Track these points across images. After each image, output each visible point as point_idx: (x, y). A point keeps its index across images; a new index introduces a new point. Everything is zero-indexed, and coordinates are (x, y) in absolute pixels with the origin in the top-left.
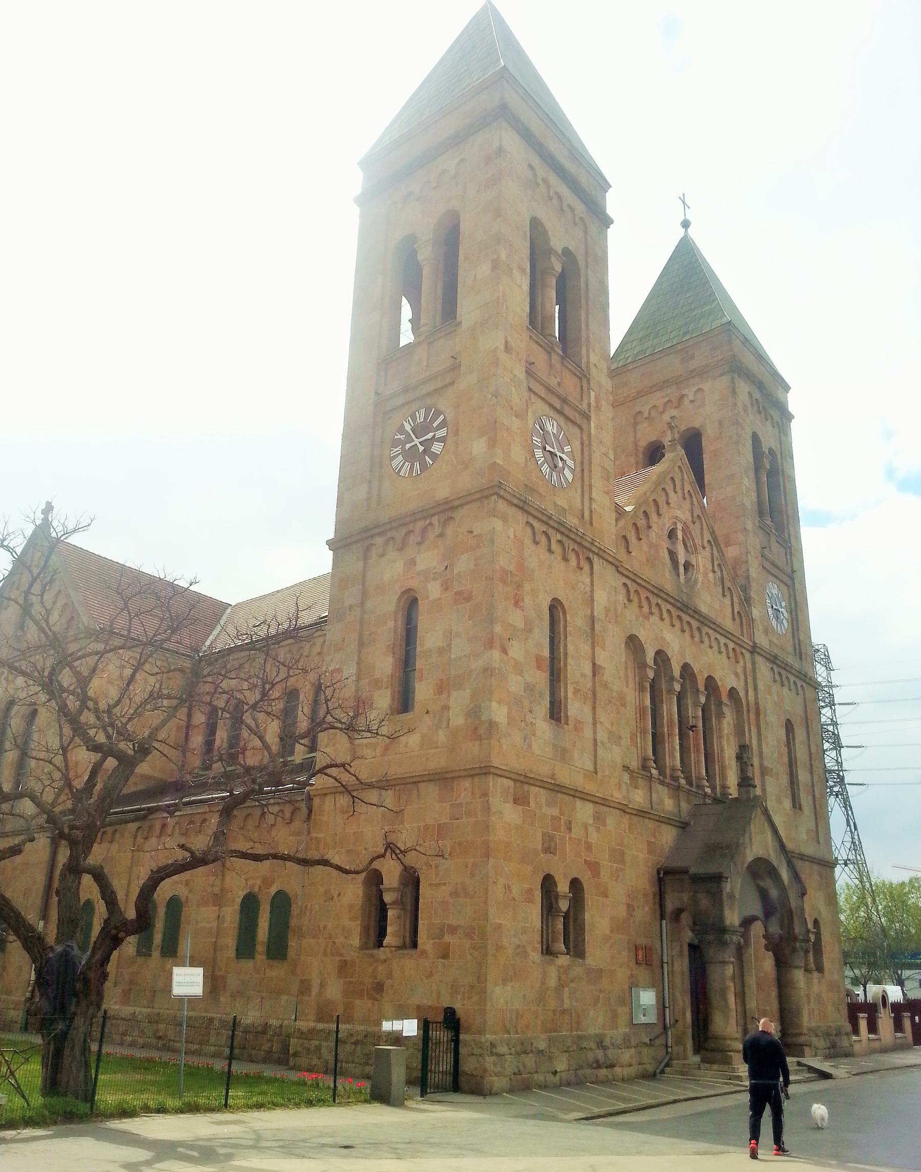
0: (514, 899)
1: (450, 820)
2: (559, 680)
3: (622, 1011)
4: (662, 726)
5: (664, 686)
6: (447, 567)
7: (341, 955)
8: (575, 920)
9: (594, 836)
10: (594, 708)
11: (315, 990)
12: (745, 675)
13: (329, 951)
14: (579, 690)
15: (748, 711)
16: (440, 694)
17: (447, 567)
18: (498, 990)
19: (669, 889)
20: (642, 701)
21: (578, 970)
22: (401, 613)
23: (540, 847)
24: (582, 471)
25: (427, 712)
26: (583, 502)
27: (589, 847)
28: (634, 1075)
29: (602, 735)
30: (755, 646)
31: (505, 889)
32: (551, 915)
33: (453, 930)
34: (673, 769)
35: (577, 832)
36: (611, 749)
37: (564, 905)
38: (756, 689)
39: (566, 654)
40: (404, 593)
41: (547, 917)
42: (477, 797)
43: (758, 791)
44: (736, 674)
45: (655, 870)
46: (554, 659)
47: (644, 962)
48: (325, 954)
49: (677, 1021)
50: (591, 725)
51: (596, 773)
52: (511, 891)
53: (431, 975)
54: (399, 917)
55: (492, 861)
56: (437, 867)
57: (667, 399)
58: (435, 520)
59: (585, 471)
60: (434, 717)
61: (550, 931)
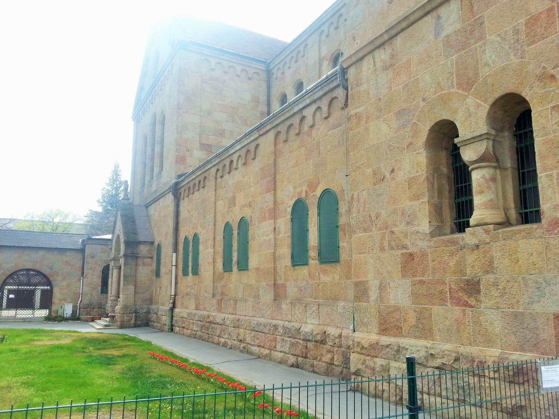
7: (405, 247)
11: (373, 294)
13: (386, 244)
48: (382, 249)
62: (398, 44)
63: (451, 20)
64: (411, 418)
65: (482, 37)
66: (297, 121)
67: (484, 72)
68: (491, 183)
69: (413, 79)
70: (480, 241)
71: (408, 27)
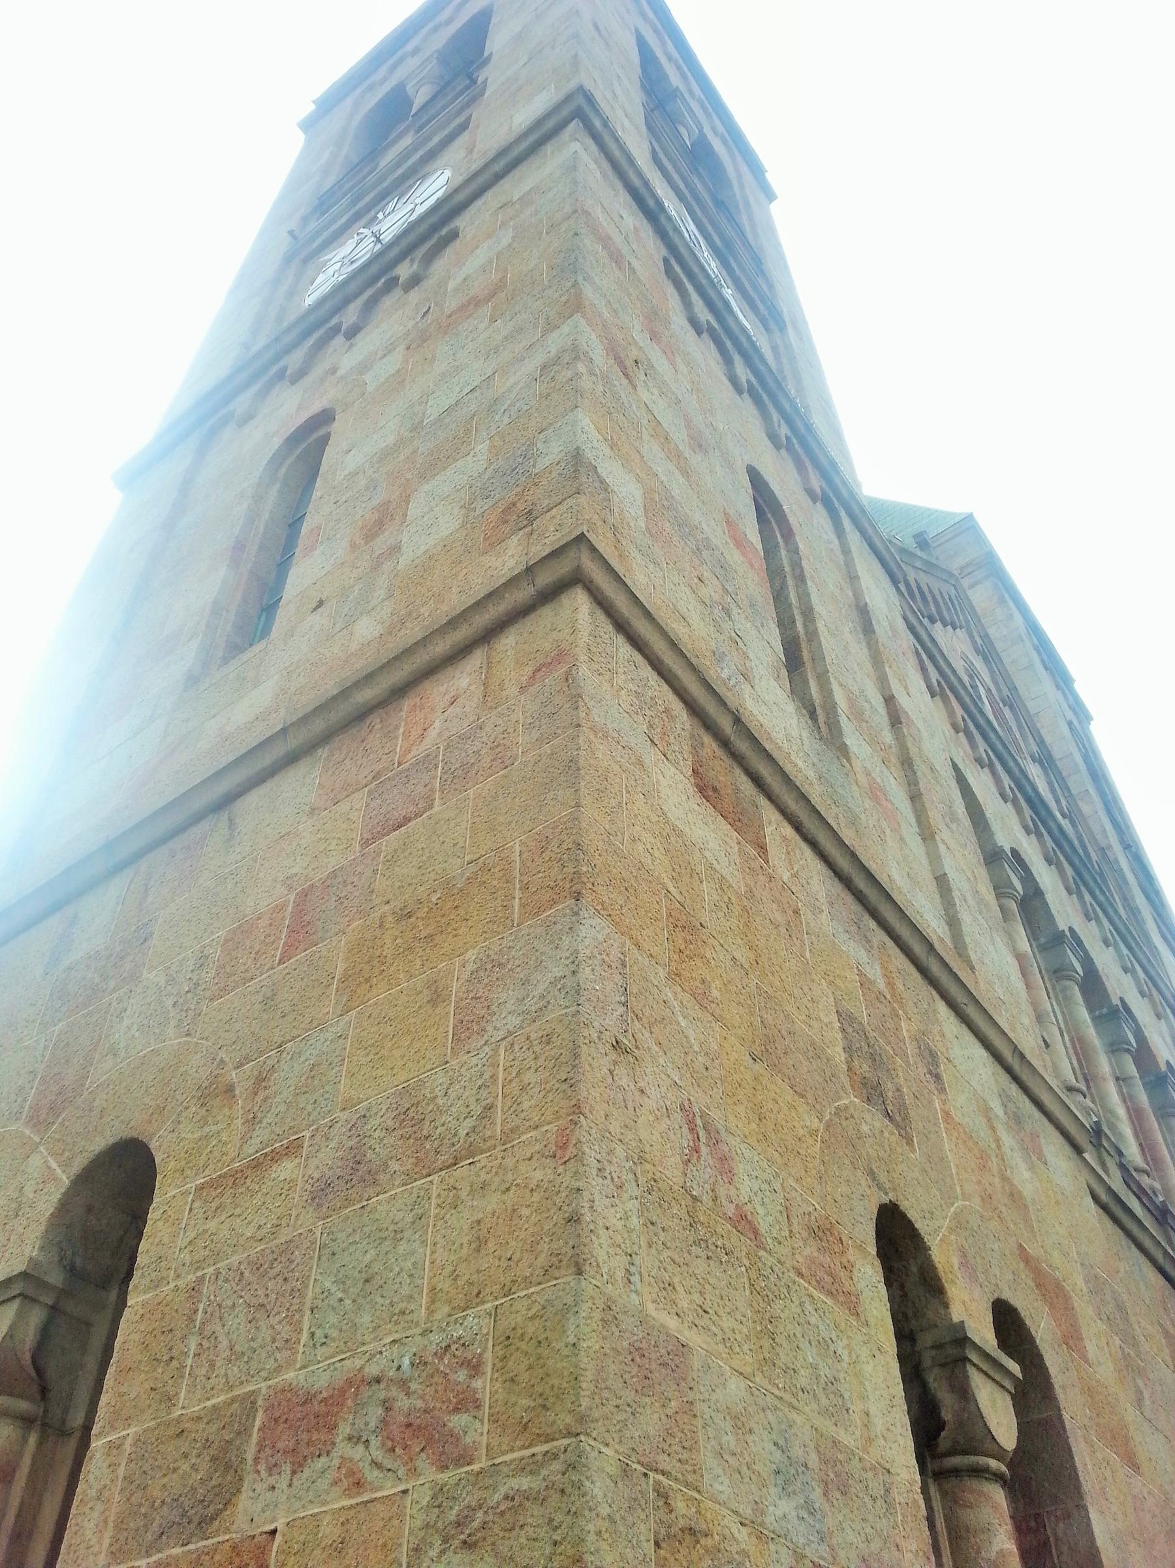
42: (511, 690)
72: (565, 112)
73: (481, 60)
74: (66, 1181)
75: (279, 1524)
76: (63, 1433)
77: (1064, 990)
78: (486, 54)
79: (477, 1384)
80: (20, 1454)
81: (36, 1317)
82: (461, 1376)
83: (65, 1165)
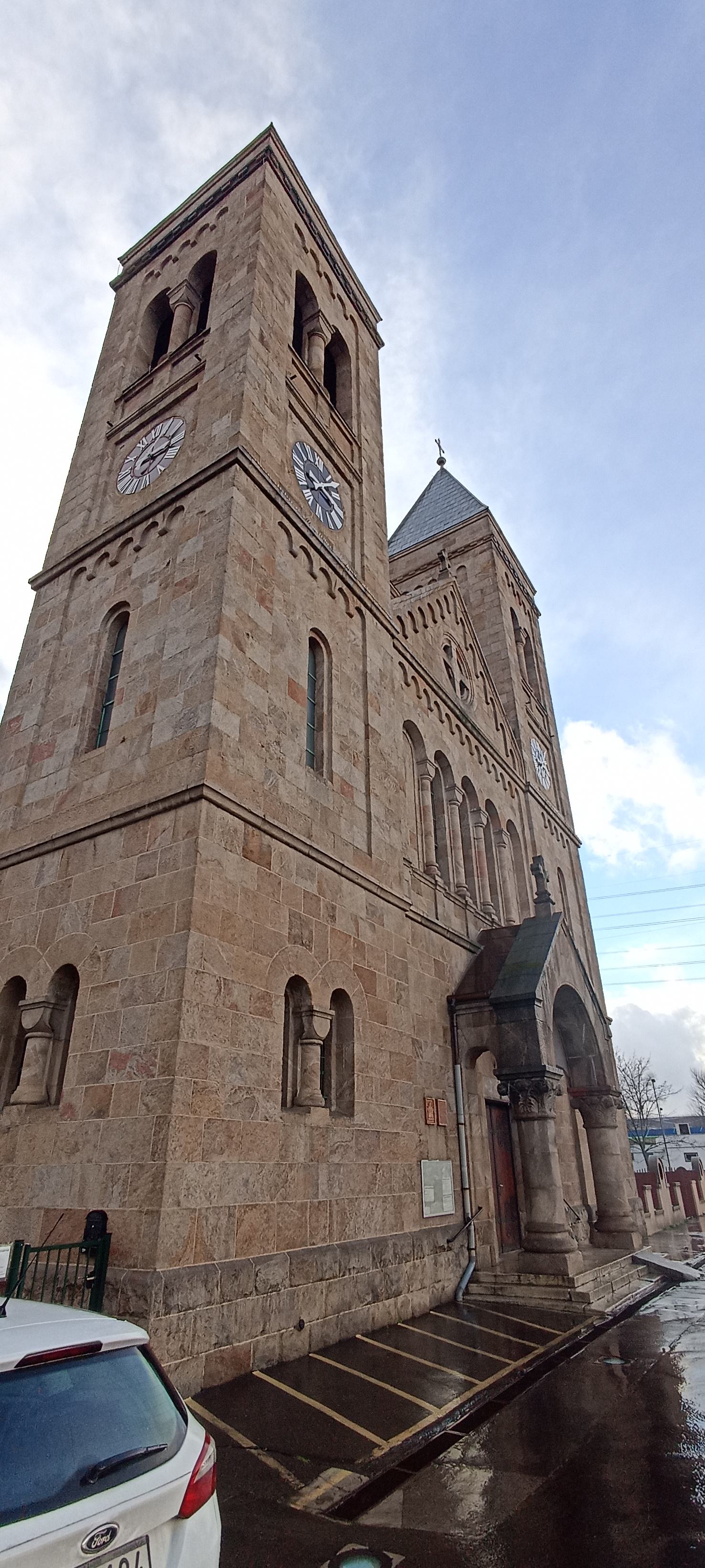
0: (234, 1006)
1: (137, 881)
2: (321, 728)
3: (408, 1196)
4: (444, 838)
5: (445, 796)
6: (168, 563)
8: (339, 1055)
9: (367, 936)
10: (367, 775)
12: (521, 812)
14: (347, 747)
15: (526, 848)
16: (142, 712)
17: (168, 563)
18: (191, 1171)
19: (462, 1021)
20: (421, 799)
21: (341, 1133)
22: (107, 635)
23: (285, 932)
24: (353, 526)
25: (124, 741)
26: (353, 557)
27: (360, 947)
28: (428, 1303)
29: (376, 809)
30: (528, 784)
31: (220, 986)
32: (302, 1044)
33: (120, 1061)
34: (458, 886)
35: (343, 923)
36: (389, 831)
37: (321, 1027)
38: (531, 828)
39: (330, 699)
40: (113, 610)
41: (296, 1043)
42: (180, 837)
43: (557, 908)
44: (512, 808)
45: (444, 999)
46: (315, 705)
47: (436, 1123)
49: (480, 1208)
50: (364, 797)
51: (370, 854)
52: (229, 993)
53: (75, 1149)
54: (44, 1052)
55: (195, 936)
56: (108, 958)
57: (431, 578)
58: (159, 518)
59: (356, 527)
60: (132, 744)
61: (299, 1070)
62: (6, 878)
63: (51, 872)
64: (381, 1567)
65: (66, 900)
66: (209, 247)
67: (60, 937)
68: (39, 1055)
69: (8, 921)
70: (11, 1123)
71: (18, 863)
72: (231, 459)
73: (204, 331)
74: (53, 973)
75: (115, 1083)
76: (59, 1040)
77: (452, 809)
78: (207, 328)
79: (156, 1060)
80: (48, 1047)
81: (49, 1011)
82: (153, 1058)
83: (53, 966)
